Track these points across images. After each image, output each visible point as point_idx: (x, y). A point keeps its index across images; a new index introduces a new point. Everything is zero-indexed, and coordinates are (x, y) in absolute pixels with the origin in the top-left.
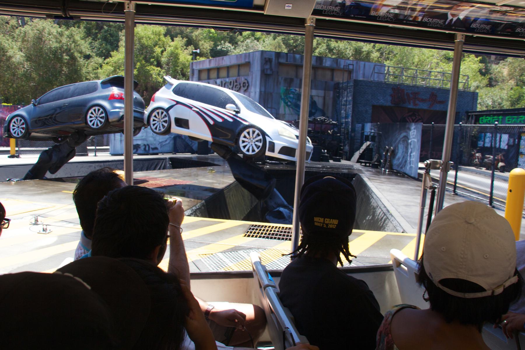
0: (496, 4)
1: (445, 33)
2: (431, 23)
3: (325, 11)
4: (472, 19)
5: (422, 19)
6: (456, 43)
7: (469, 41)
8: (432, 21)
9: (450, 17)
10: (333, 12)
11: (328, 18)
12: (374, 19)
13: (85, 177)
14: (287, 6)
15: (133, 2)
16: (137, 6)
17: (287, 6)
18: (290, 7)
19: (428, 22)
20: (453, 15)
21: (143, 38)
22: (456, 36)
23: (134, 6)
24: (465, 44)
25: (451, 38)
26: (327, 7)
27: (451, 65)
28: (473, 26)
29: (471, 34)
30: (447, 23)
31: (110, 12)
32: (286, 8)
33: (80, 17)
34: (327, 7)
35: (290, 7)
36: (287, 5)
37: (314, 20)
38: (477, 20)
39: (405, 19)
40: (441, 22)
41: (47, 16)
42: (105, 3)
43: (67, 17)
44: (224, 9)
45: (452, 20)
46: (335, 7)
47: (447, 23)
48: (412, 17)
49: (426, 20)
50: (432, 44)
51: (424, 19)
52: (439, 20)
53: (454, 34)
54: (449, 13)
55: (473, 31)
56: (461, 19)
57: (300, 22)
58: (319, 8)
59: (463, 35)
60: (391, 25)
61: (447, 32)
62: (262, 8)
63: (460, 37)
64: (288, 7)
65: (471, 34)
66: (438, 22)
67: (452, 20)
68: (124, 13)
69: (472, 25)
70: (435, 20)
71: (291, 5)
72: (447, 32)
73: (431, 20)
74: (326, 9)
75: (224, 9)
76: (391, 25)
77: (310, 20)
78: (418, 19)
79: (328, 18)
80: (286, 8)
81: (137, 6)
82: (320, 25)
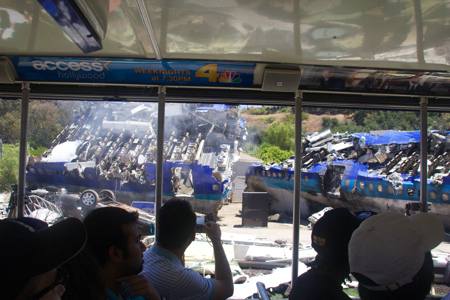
0: (448, 72)
1: (410, 97)
2: (396, 90)
3: (309, 86)
4: (431, 85)
5: (388, 87)
6: (421, 105)
7: (432, 102)
8: (438, 90)
9: (412, 85)
10: (315, 86)
11: (312, 92)
12: (349, 90)
13: (241, 269)
14: (278, 84)
15: (165, 87)
16: (167, 89)
17: (278, 84)
18: (281, 84)
19: (436, 92)
20: (414, 83)
21: (328, 121)
22: (420, 99)
23: (165, 89)
24: (303, 100)
25: (416, 101)
26: (310, 83)
27: (18, 105)
28: (433, 90)
29: (433, 97)
30: (410, 89)
31: (147, 94)
32: (278, 85)
33: (126, 99)
34: (310, 83)
35: (281, 84)
36: (278, 83)
37: (301, 94)
38: (436, 85)
39: (374, 88)
40: (405, 88)
41: (103, 99)
42: (144, 88)
43: (118, 99)
44: (232, 88)
45: (414, 86)
46: (317, 83)
47: (410, 89)
48: (380, 86)
49: (391, 88)
50: (248, 101)
51: (390, 87)
52: (403, 87)
53: (419, 97)
54: (410, 81)
55: (434, 94)
56: (422, 85)
57: (290, 96)
58: (304, 84)
59: (426, 98)
60: (364, 94)
61: (412, 96)
62: (260, 86)
63: (423, 99)
64: (280, 84)
65: (433, 97)
66: (402, 89)
67: (414, 86)
68: (157, 95)
69: (432, 89)
70: (399, 88)
71: (281, 83)
72: (412, 96)
73: (395, 87)
74: (310, 84)
75: (232, 88)
76: (364, 94)
77: (298, 94)
78: (385, 87)
79: (312, 92)
80: (278, 85)
81: (167, 89)
82: (307, 97)
